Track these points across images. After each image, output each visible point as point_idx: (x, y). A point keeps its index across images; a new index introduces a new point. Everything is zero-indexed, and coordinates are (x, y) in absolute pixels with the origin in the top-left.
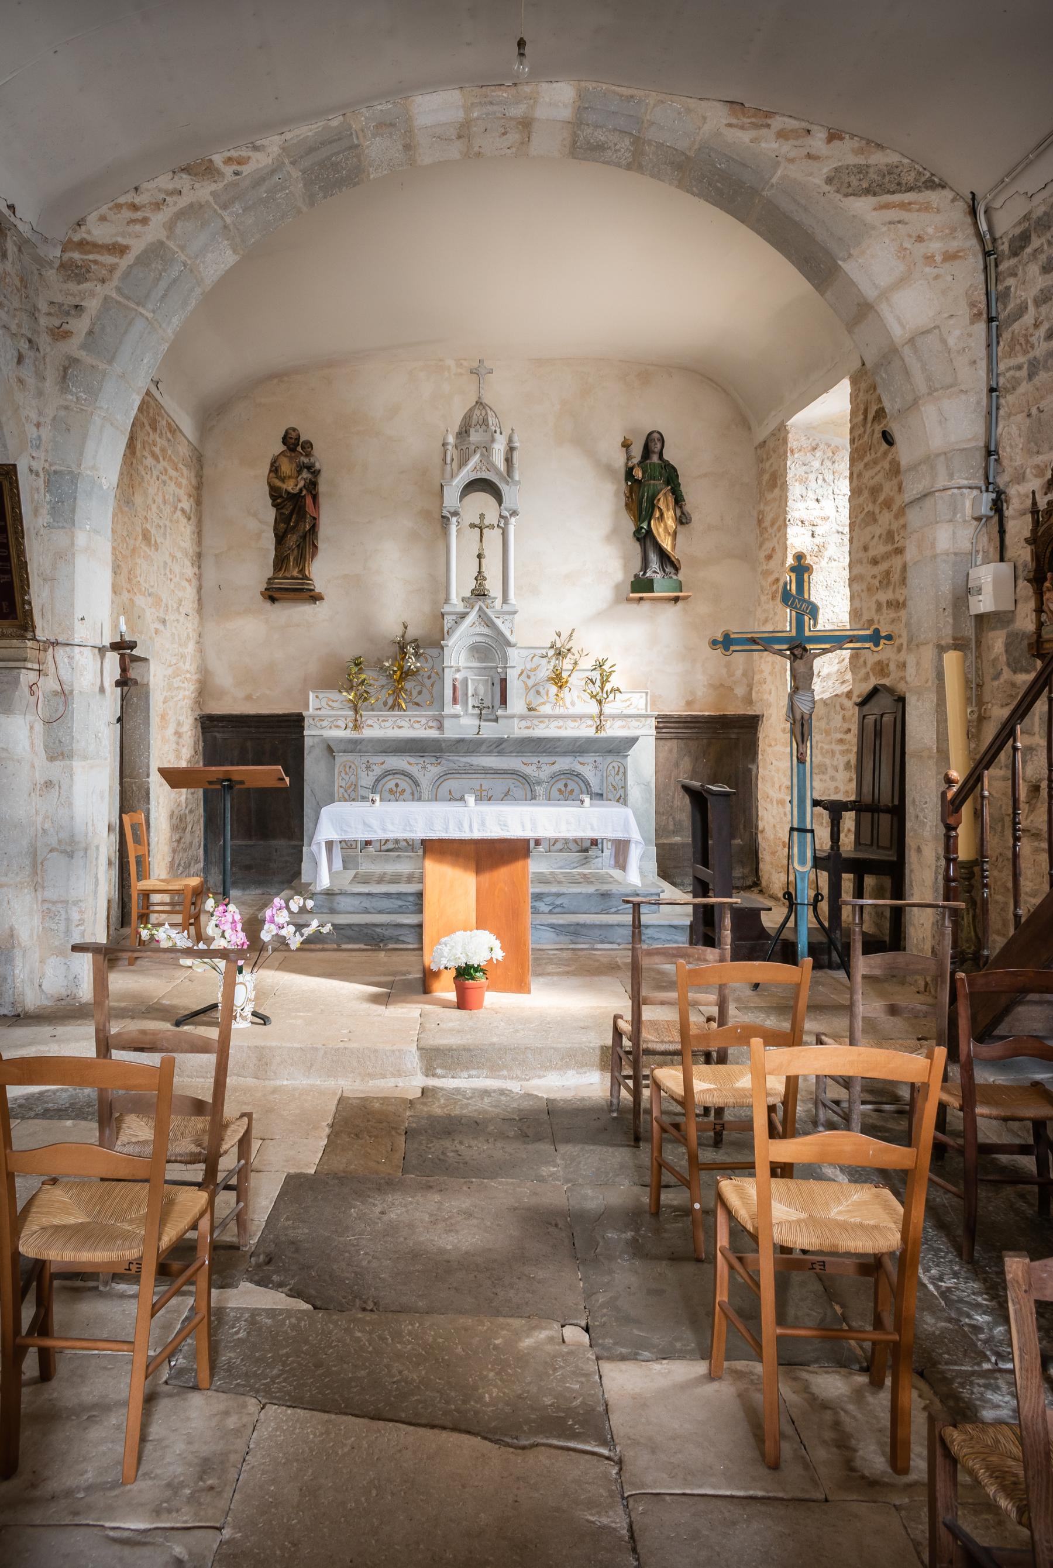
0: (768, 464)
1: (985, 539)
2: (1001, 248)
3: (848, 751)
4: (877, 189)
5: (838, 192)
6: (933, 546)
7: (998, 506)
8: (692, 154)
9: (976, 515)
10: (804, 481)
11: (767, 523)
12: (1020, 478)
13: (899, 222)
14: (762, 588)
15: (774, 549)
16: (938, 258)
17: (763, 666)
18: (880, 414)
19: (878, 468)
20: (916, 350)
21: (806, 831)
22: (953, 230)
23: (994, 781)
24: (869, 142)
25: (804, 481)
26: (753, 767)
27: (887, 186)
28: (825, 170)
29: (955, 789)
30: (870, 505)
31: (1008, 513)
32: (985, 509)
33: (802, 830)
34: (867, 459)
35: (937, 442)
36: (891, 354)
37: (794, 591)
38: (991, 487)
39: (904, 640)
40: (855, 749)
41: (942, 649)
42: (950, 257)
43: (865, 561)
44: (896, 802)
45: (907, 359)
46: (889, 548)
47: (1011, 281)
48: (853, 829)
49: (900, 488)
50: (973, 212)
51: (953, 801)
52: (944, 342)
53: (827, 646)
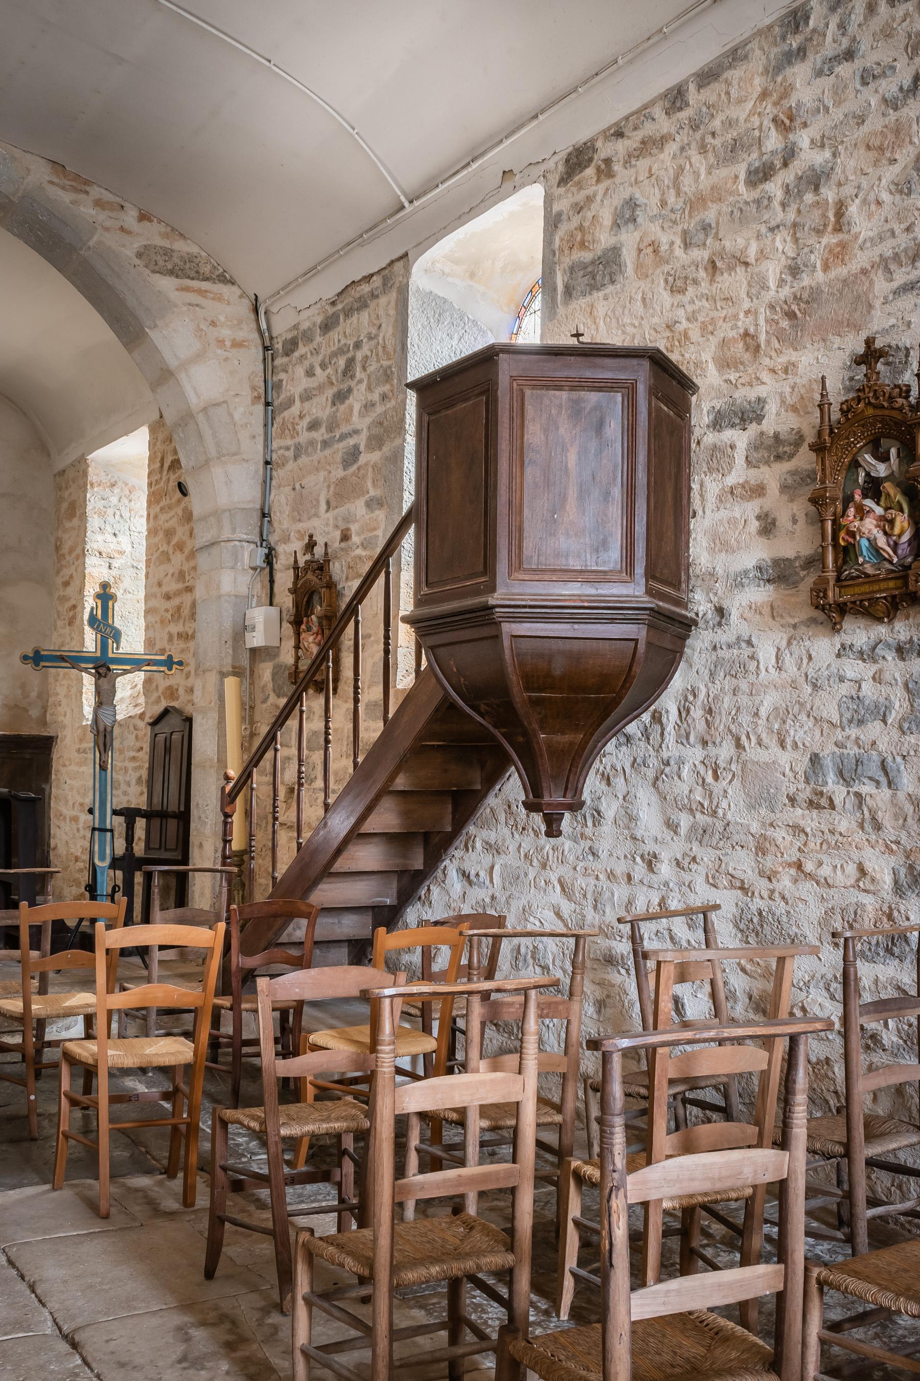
0: (66, 494)
1: (259, 586)
2: (276, 346)
3: (140, 767)
4: (180, 273)
5: (146, 267)
6: (218, 588)
7: (270, 559)
8: (15, 200)
9: (253, 565)
10: (102, 514)
11: (65, 550)
12: (286, 539)
13: (197, 305)
14: (58, 612)
15: (71, 576)
16: (228, 344)
17: (59, 689)
18: (176, 465)
19: (172, 513)
20: (208, 419)
21: (106, 830)
22: (240, 322)
23: (259, 779)
24: (173, 229)
25: (102, 514)
26: (47, 787)
27: (188, 272)
28: (136, 245)
29: (231, 785)
30: (165, 546)
31: (276, 566)
32: (259, 561)
33: (103, 830)
34: (162, 504)
35: (223, 501)
36: (187, 417)
37: (99, 616)
38: (264, 544)
39: (191, 668)
40: (147, 765)
41: (223, 675)
42: (237, 344)
43: (159, 595)
44: (182, 809)
45: (201, 425)
46: (181, 586)
47: (282, 376)
48: (143, 837)
49: (191, 534)
50: (256, 310)
51: (230, 794)
52: (231, 415)
53: (128, 667)
